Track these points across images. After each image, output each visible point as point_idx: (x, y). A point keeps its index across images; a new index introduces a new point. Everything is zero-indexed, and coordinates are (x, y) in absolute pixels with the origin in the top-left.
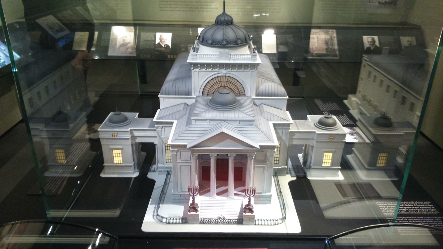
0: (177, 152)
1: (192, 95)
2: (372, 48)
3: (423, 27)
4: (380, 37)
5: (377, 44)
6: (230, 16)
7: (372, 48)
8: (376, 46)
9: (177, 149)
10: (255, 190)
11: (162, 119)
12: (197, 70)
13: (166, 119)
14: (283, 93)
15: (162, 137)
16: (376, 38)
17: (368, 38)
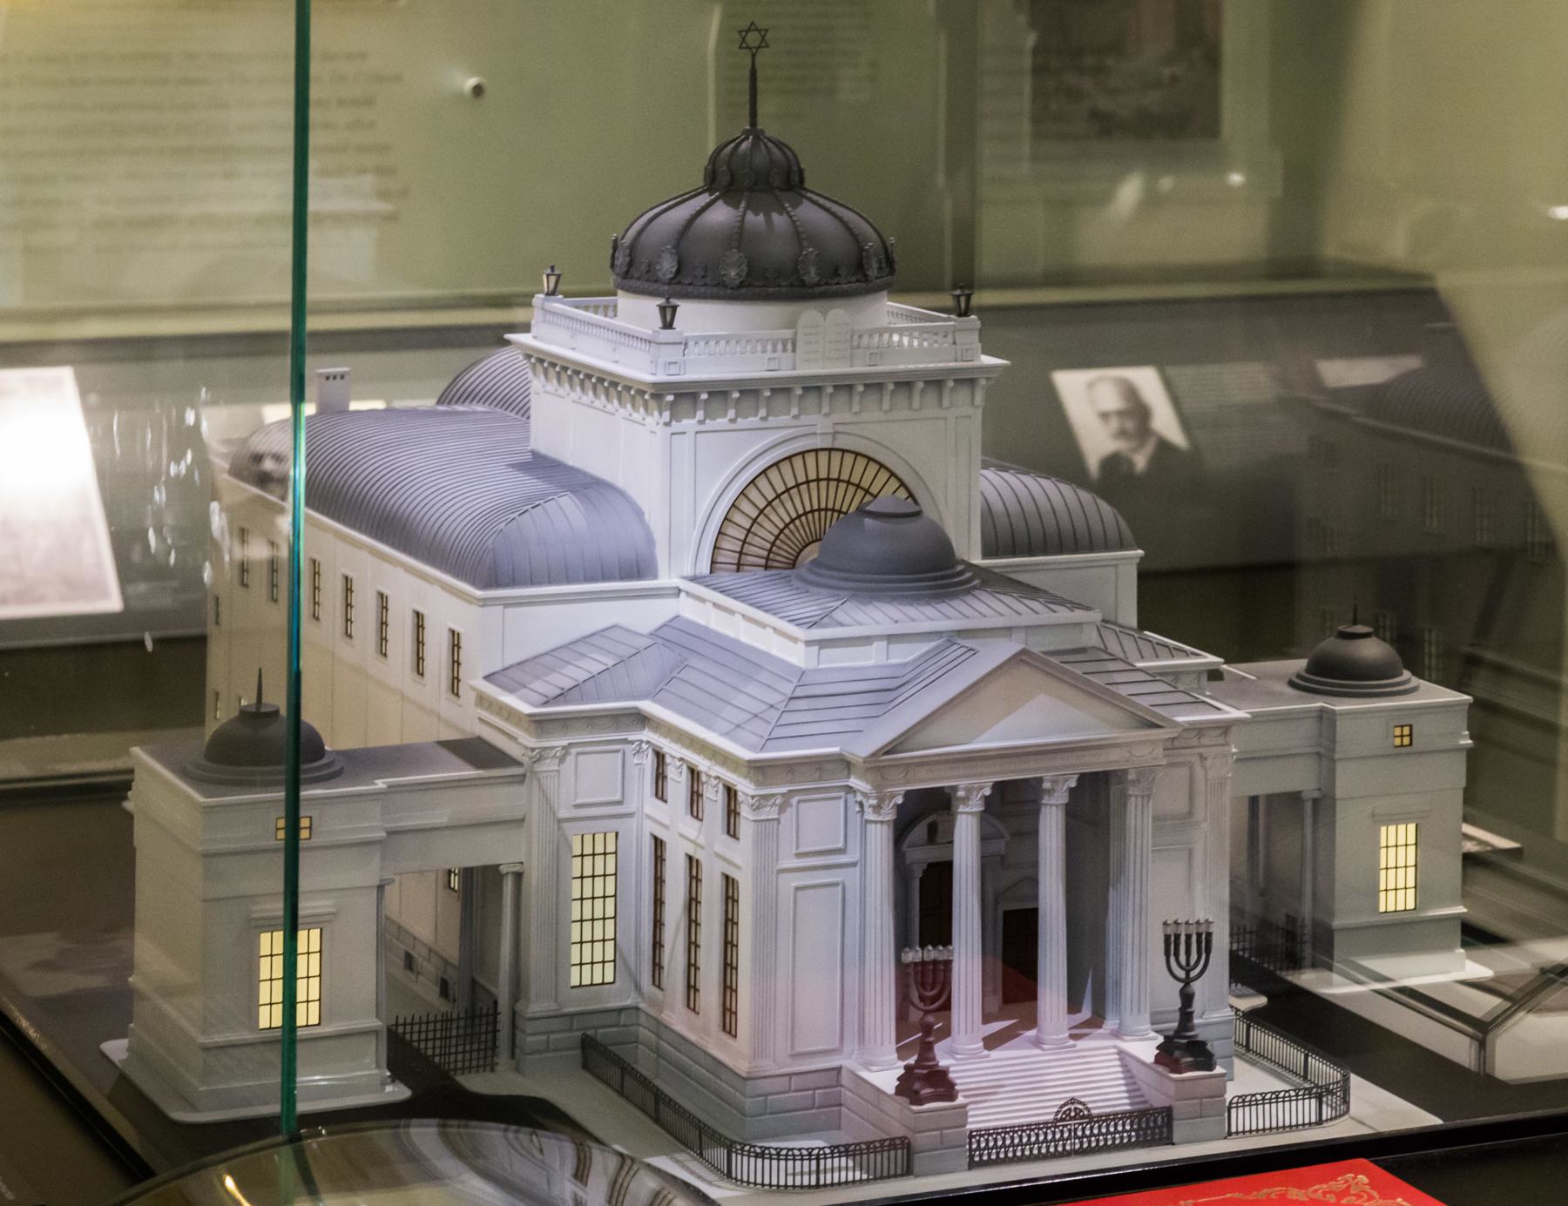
0: (782, 808)
1: (655, 577)
2: (1141, 461)
3: (1445, 282)
4: (1172, 371)
5: (1166, 422)
6: (779, 145)
7: (1141, 461)
8: (1164, 446)
9: (784, 790)
10: (1209, 935)
11: (566, 703)
12: (689, 424)
13: (582, 701)
14: (1112, 533)
15: (563, 814)
16: (1147, 380)
17: (1091, 385)
